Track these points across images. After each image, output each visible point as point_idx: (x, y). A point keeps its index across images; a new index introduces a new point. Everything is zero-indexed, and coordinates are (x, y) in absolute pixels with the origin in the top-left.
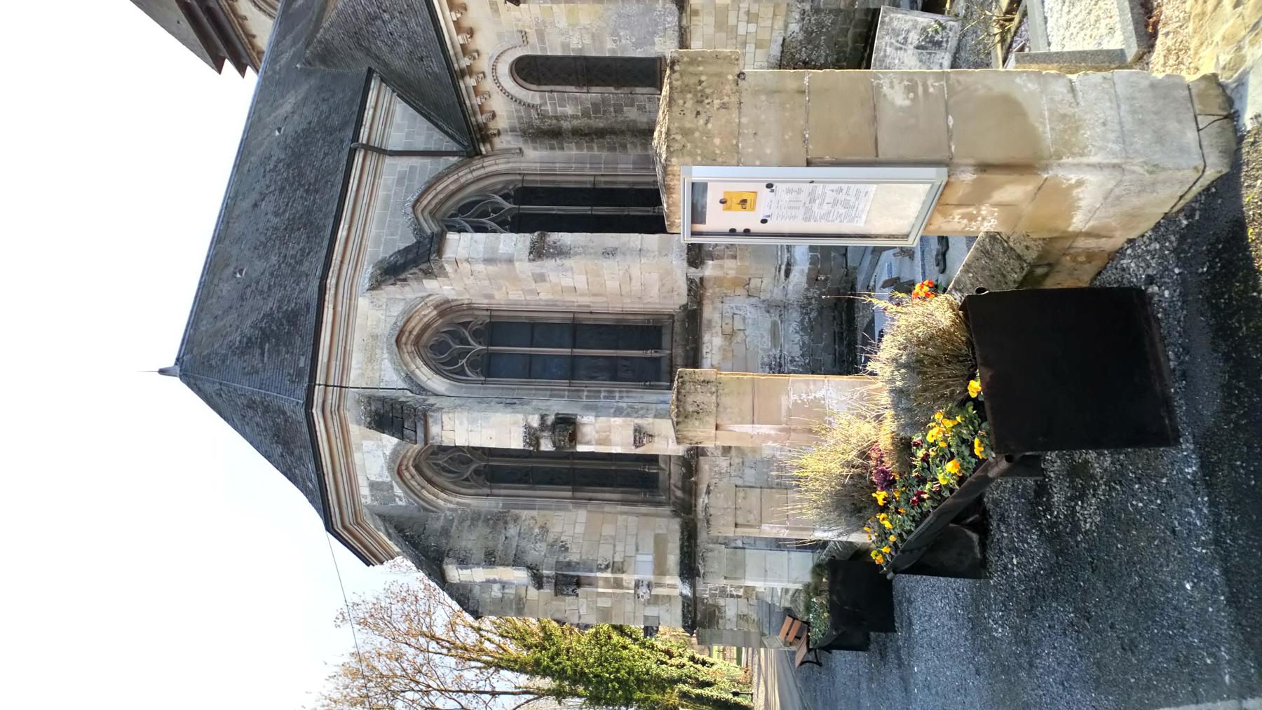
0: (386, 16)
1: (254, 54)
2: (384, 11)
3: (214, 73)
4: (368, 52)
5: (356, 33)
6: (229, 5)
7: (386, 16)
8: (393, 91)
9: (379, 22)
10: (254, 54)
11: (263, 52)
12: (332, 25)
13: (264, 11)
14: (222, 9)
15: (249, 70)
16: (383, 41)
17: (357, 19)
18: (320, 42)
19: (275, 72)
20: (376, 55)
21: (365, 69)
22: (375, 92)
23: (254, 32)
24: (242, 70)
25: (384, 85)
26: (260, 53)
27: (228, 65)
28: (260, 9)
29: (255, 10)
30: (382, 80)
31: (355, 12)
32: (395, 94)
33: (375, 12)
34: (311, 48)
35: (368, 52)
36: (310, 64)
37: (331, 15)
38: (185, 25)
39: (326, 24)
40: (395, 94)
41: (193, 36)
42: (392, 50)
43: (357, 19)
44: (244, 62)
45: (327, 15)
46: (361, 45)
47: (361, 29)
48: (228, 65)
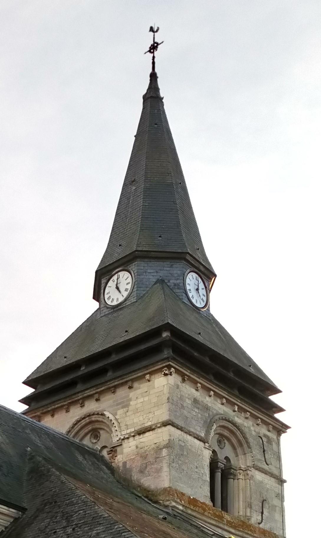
0: (69, 530)
1: (38, 414)
2: (74, 529)
3: (24, 378)
4: (40, 510)
5: (56, 502)
6: (79, 400)
7: (69, 530)
8: (6, 528)
9: (64, 523)
10: (38, 414)
11: (39, 421)
12: (62, 482)
13: (73, 427)
14: (75, 394)
15: (25, 407)
16: (49, 524)
17: (67, 505)
18: (49, 471)
19: (24, 428)
20: (37, 516)
21: (25, 505)
22: (6, 512)
23: (56, 416)
24: (24, 401)
25: (12, 520)
26: (39, 419)
27: (29, 391)
28: (75, 424)
29: (74, 420)
30: (16, 519)
31: (72, 504)
32: (3, 529)
33: (73, 521)
34: (43, 462)
35: (40, 510)
36: (30, 459)
37: (72, 483)
38: (63, 363)
39: (63, 477)
40: (3, 529)
41: (55, 367)
42: (42, 531)
43: (67, 505)
44: (33, 404)
45: (70, 479)
46: (45, 505)
47: (59, 507)
48: (29, 391)
